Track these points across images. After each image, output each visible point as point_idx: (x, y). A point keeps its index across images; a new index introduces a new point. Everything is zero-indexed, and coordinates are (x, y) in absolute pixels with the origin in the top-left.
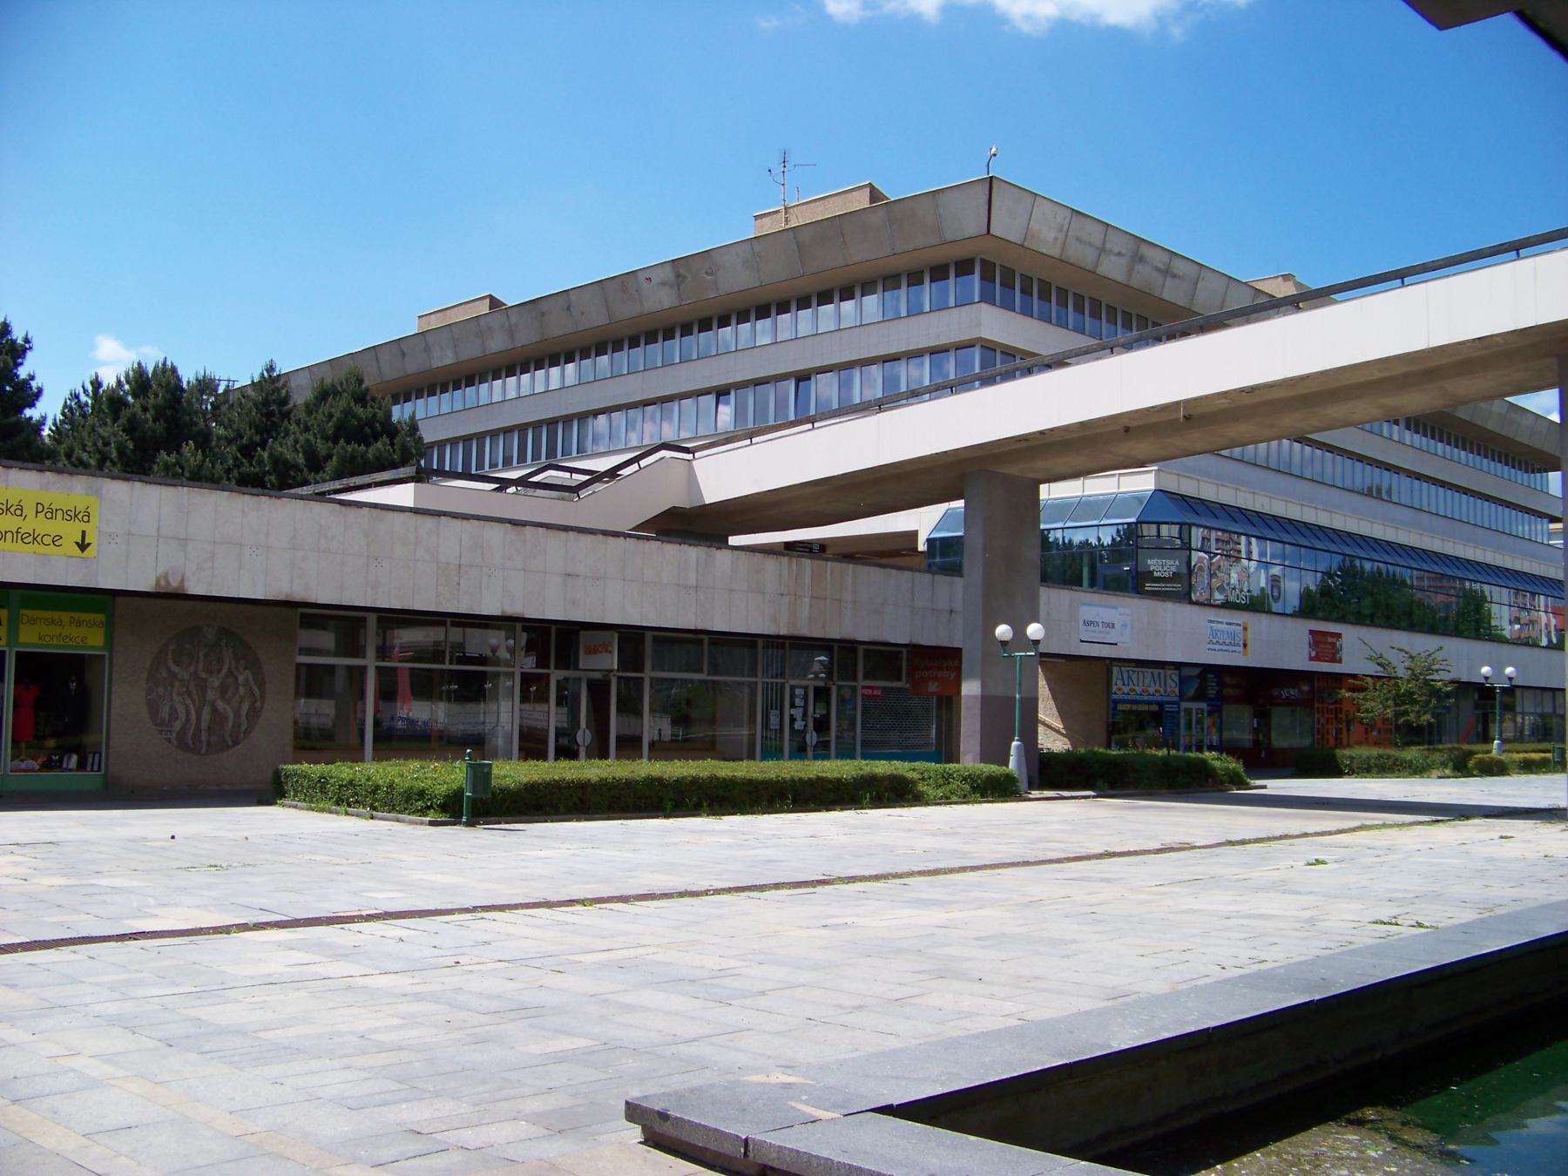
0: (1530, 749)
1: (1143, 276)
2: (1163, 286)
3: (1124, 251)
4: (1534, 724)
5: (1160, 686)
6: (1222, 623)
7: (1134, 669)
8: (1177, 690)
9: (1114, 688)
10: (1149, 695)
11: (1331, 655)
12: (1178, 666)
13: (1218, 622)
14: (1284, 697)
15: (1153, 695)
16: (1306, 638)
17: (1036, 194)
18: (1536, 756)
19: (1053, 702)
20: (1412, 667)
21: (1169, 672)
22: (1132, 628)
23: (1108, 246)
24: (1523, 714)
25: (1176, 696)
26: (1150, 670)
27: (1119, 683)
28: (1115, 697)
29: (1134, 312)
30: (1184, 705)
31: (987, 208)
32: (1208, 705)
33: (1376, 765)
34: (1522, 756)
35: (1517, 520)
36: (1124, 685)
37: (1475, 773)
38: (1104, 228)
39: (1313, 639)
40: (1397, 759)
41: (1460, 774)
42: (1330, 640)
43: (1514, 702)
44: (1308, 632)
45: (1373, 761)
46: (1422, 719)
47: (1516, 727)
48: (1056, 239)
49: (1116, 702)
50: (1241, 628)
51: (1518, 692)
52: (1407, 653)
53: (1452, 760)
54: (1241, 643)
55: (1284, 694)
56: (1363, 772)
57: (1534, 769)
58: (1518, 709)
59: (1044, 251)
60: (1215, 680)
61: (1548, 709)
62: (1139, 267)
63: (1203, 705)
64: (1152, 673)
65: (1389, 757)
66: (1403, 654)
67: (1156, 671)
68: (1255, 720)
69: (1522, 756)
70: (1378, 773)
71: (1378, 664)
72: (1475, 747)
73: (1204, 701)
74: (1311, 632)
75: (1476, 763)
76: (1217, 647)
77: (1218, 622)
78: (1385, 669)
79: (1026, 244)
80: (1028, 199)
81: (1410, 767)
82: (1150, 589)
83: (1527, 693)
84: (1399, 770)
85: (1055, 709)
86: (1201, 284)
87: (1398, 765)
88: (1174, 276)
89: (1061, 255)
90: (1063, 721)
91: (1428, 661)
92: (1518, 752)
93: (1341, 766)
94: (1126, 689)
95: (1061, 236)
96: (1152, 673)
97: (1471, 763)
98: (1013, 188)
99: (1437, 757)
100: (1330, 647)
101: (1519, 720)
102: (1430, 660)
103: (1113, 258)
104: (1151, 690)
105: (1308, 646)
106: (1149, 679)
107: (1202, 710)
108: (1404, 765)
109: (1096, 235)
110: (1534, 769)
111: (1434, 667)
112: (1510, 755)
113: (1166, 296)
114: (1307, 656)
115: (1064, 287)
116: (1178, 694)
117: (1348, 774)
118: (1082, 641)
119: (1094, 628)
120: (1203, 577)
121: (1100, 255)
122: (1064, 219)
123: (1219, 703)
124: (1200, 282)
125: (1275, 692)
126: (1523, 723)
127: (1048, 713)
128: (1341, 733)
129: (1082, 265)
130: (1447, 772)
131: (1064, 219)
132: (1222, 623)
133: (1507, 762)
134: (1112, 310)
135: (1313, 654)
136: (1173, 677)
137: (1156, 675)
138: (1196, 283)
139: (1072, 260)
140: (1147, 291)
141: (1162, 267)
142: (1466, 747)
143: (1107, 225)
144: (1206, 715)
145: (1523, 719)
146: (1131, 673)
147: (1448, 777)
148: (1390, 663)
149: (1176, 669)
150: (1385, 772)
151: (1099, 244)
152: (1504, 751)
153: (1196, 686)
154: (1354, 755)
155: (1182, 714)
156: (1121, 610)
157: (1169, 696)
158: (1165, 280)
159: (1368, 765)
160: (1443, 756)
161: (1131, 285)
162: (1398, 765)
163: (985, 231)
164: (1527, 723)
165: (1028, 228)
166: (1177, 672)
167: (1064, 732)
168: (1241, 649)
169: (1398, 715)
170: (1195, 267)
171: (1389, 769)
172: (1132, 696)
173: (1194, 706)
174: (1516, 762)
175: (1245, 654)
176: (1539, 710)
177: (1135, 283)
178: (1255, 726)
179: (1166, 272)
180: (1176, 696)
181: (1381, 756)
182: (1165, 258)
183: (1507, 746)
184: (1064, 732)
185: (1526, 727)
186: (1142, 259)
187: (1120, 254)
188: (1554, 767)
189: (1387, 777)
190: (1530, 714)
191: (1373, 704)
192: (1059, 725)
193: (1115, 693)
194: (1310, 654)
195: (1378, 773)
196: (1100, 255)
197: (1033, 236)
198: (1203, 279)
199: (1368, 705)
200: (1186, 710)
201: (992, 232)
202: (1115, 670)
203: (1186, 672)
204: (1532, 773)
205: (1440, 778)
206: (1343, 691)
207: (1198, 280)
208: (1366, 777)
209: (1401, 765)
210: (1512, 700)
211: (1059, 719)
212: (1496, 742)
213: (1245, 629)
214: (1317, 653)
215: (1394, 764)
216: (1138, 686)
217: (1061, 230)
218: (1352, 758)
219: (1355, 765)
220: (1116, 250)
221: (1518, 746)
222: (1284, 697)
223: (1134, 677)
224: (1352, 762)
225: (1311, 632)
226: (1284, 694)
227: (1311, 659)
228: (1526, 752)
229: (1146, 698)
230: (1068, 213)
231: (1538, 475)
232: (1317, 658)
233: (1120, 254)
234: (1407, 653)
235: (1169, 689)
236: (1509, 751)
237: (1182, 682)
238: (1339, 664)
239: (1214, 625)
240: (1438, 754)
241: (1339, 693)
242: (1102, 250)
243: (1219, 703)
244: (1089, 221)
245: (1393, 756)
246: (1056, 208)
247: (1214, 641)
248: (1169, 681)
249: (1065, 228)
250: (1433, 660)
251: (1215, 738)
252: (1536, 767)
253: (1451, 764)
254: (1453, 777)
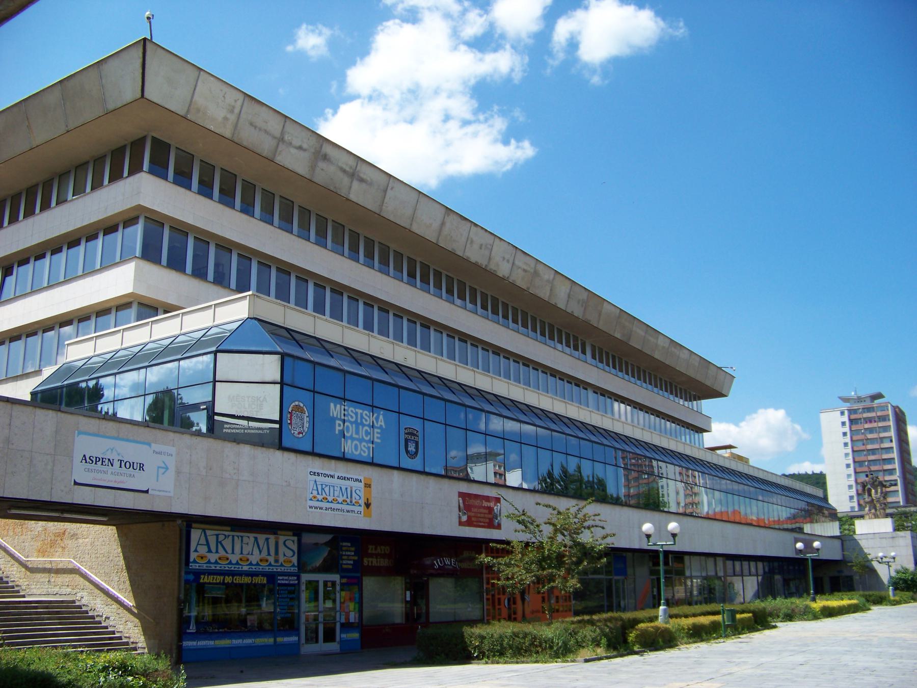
0: (699, 611)
1: (325, 174)
2: (350, 188)
3: (305, 146)
4: (701, 585)
5: (269, 554)
6: (332, 477)
7: (227, 533)
8: (295, 560)
9: (193, 556)
10: (251, 564)
11: (487, 520)
12: (298, 530)
13: (326, 475)
14: (437, 566)
15: (258, 564)
16: (455, 501)
17: (201, 70)
18: (705, 620)
19: (126, 574)
20: (553, 521)
21: (282, 539)
22: (178, 472)
23: (286, 138)
24: (691, 577)
25: (293, 566)
26: (252, 536)
27: (203, 550)
28: (193, 566)
29: (330, 218)
30: (305, 577)
31: (141, 71)
32: (342, 577)
33: (511, 647)
34: (691, 621)
35: (680, 433)
36: (210, 551)
37: (636, 649)
38: (284, 120)
39: (464, 503)
40: (535, 638)
41: (615, 653)
42: (485, 504)
43: (684, 568)
44: (457, 494)
45: (506, 640)
46: (568, 584)
47: (686, 589)
48: (226, 119)
49: (198, 574)
50: (362, 485)
51: (686, 558)
52: (554, 509)
53: (606, 635)
54: (362, 502)
55: (437, 563)
56: (494, 656)
57: (704, 637)
58: (688, 573)
59: (212, 128)
60: (353, 549)
61: (711, 573)
62: (321, 165)
63: (336, 577)
64: (256, 538)
65: (526, 635)
66: (550, 510)
67: (262, 538)
68: (408, 593)
69: (691, 621)
70: (512, 657)
71: (519, 522)
72: (639, 614)
73: (337, 572)
74: (461, 495)
75: (637, 637)
76: (325, 505)
77: (326, 475)
78: (526, 527)
79: (189, 117)
80: (194, 73)
81: (551, 647)
82: (229, 431)
83: (695, 559)
84: (537, 652)
85: (128, 582)
86: (390, 193)
87: (536, 646)
88: (362, 180)
89: (233, 134)
90: (135, 597)
91: (579, 516)
92: (686, 616)
93: (470, 649)
94: (213, 557)
95: (232, 118)
96: (256, 538)
97: (632, 636)
98: (172, 56)
99: (588, 632)
100: (487, 511)
101: (689, 583)
102: (580, 516)
103: (293, 151)
104: (254, 559)
105: (457, 509)
106: (251, 545)
107: (334, 583)
108: (544, 644)
109: (275, 125)
110: (704, 637)
111: (586, 524)
112: (678, 620)
113: (353, 197)
114: (457, 520)
115: (252, 181)
116: (296, 564)
117: (478, 658)
118: (76, 483)
119: (104, 468)
120: (302, 419)
121: (278, 145)
122: (236, 101)
123: (358, 575)
124: (389, 191)
125: (428, 561)
126: (692, 585)
127: (121, 587)
128: (515, 603)
129: (259, 151)
130: (600, 651)
131: (236, 101)
132: (332, 477)
133: (674, 630)
134: (305, 213)
135: (464, 518)
136: (289, 543)
137: (261, 542)
138: (385, 191)
139: (245, 144)
140: (332, 188)
141: (348, 169)
142: (628, 615)
143: (286, 117)
144: (338, 588)
145: (692, 582)
146: (221, 538)
147: (600, 659)
148: (534, 521)
149: (294, 535)
150: (521, 654)
151: (278, 135)
152: (671, 617)
153: (325, 554)
154: (484, 634)
155: (303, 587)
156: (155, 447)
157: (282, 565)
158: (352, 182)
159: (502, 645)
160: (594, 631)
161: (315, 180)
162: (536, 646)
163: (139, 95)
164: (695, 585)
165: (191, 101)
166: (296, 538)
167: (136, 611)
168: (362, 509)
169: (539, 581)
170: (384, 176)
171: (526, 651)
172: (224, 566)
173: (321, 578)
174: (683, 629)
175: (368, 515)
176: (704, 574)
177: (319, 178)
178: (408, 599)
179: (353, 175)
180: (293, 566)
181: (515, 635)
182: (352, 162)
183: (675, 610)
184: (136, 611)
185: (695, 589)
186: (325, 158)
187: (300, 148)
188: (725, 631)
189: (523, 662)
190: (697, 577)
191: (516, 569)
192: (130, 602)
193: (195, 561)
194: (460, 517)
195: (514, 655)
196: (278, 145)
197: (198, 110)
198: (392, 188)
199: (509, 571)
200: (309, 583)
201: (146, 95)
202: (195, 535)
203: (308, 539)
204: (702, 640)
205: (587, 661)
206: (483, 556)
207: (387, 189)
208: (498, 663)
209: (540, 646)
210: (680, 565)
211: (131, 594)
212: (662, 608)
213: (368, 486)
214: (469, 517)
215: (532, 644)
216: (233, 553)
217: (232, 111)
218: (482, 638)
219: (486, 647)
220: (297, 143)
221: (686, 609)
222: (437, 566)
223: (227, 544)
224: (482, 642)
225: (461, 495)
226: (437, 563)
227: (461, 523)
228: (694, 615)
229: (245, 568)
230: (241, 97)
231: (695, 402)
232: (469, 523)
233: (300, 148)
234: (554, 509)
235: (282, 559)
236: (677, 616)
237: (301, 551)
238: (497, 531)
239: (320, 479)
240: (589, 627)
241: (477, 558)
242: (281, 140)
243: (358, 575)
244: (264, 108)
245: (530, 633)
246: (225, 89)
247: (320, 497)
248: (282, 549)
249: (237, 111)
250: (585, 516)
251: (353, 617)
252: (706, 633)
253: (604, 641)
254: (608, 658)
